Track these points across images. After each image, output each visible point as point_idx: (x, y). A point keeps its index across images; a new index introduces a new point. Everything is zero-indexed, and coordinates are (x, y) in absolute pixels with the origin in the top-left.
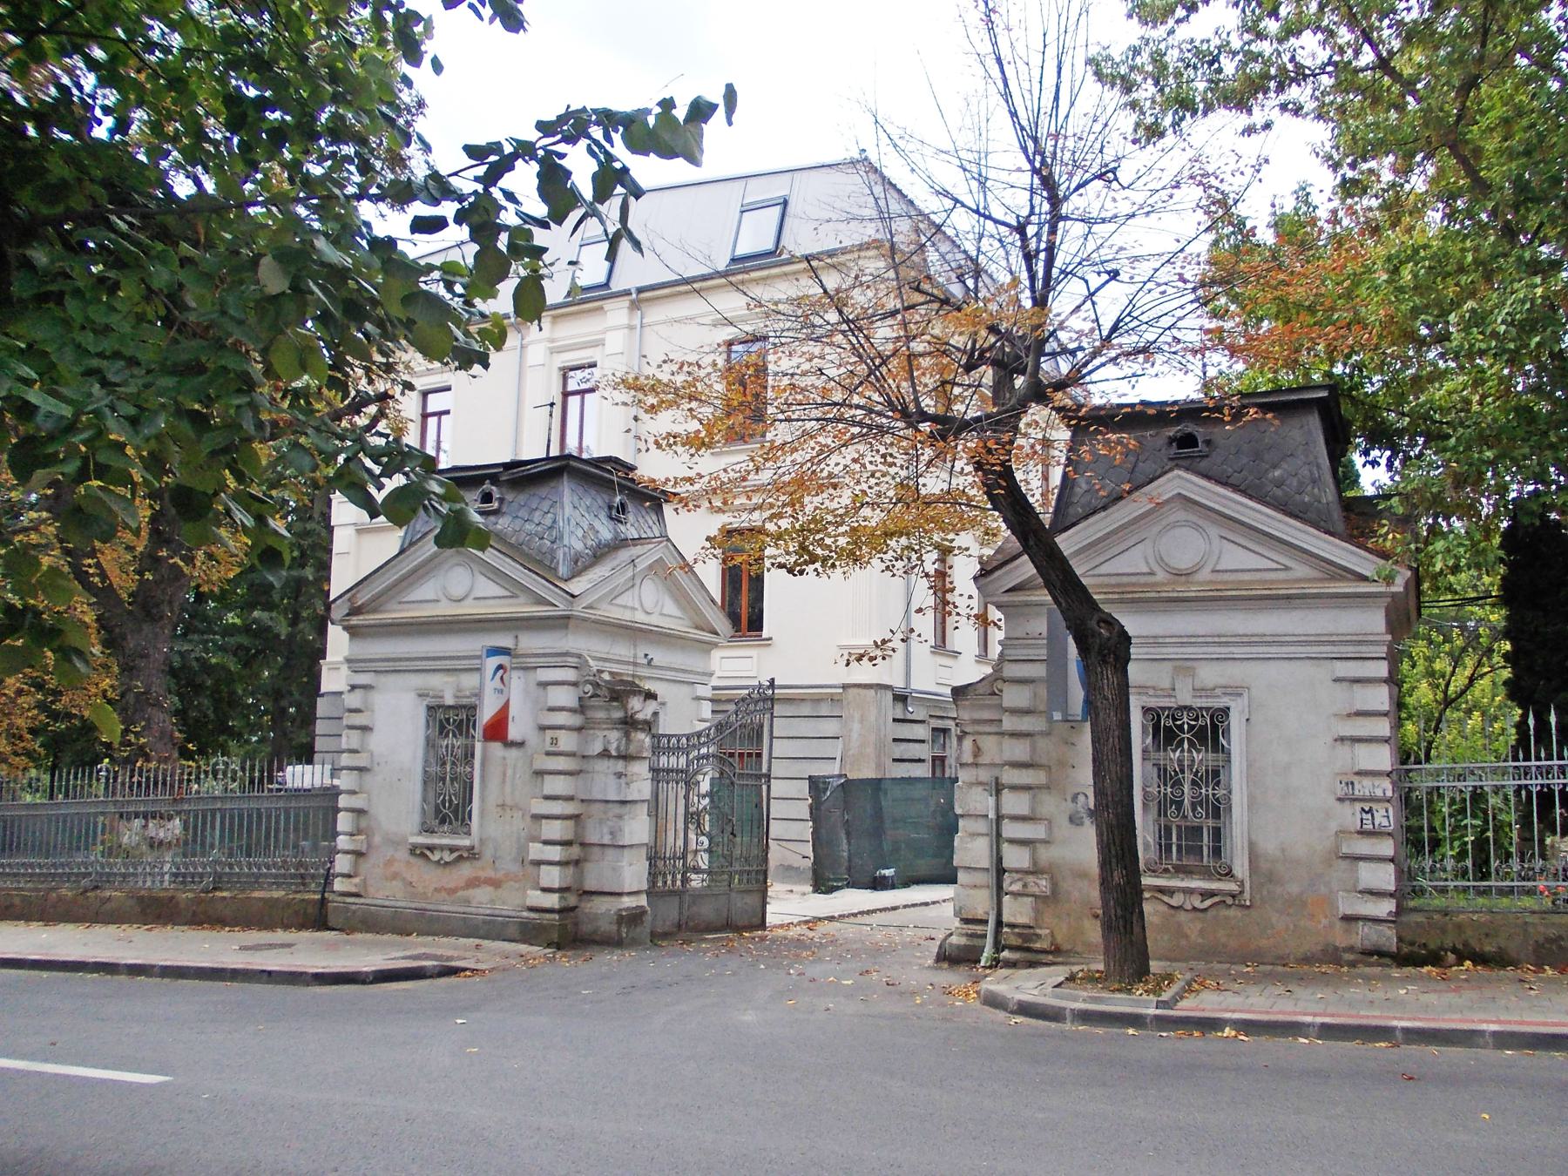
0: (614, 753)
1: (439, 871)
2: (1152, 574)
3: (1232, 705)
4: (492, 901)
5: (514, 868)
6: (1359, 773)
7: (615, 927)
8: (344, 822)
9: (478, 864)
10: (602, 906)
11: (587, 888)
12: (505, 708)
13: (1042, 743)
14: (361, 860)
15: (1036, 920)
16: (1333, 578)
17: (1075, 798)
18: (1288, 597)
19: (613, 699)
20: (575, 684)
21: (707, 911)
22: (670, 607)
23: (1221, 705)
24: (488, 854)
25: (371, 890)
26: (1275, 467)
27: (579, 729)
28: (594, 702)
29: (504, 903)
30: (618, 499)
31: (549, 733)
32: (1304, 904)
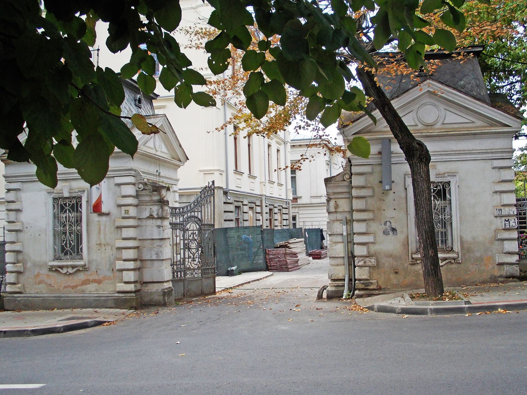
0: (156, 216)
1: (67, 277)
2: (416, 125)
3: (451, 180)
4: (97, 290)
5: (109, 274)
6: (504, 205)
7: (161, 298)
8: (9, 257)
9: (88, 273)
10: (154, 288)
11: (145, 280)
12: (100, 197)
13: (370, 200)
14: (21, 276)
15: (370, 276)
16: (491, 126)
17: (385, 224)
18: (475, 134)
19: (154, 191)
20: (134, 184)
21: (194, 287)
22: (164, 149)
23: (447, 181)
24: (93, 268)
25: (28, 290)
26: (461, 80)
27: (136, 206)
28: (144, 192)
29: (103, 291)
30: (138, 96)
31: (123, 208)
32: (482, 260)
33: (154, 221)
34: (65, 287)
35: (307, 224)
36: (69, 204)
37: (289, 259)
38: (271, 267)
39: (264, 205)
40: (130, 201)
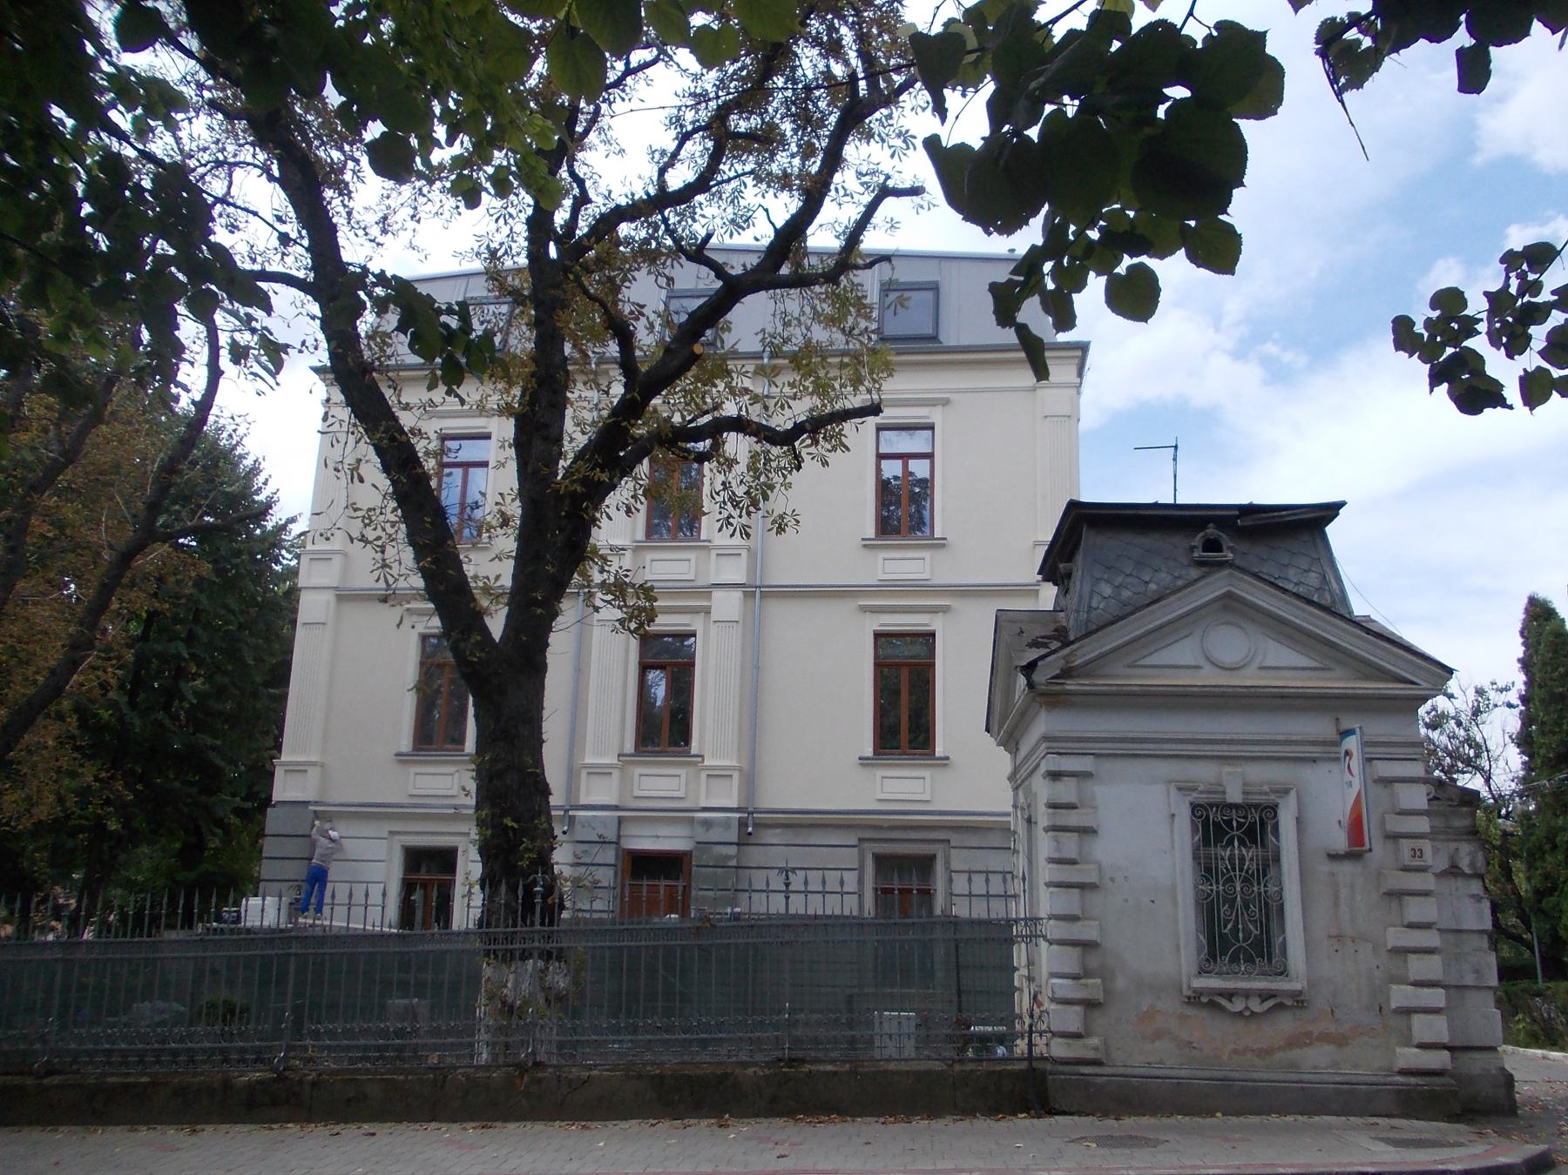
0: (1467, 871)
4: (1335, 1064)
31: (1406, 845)
33: (1460, 882)
34: (1235, 1052)
36: (1240, 825)
40: (1423, 824)
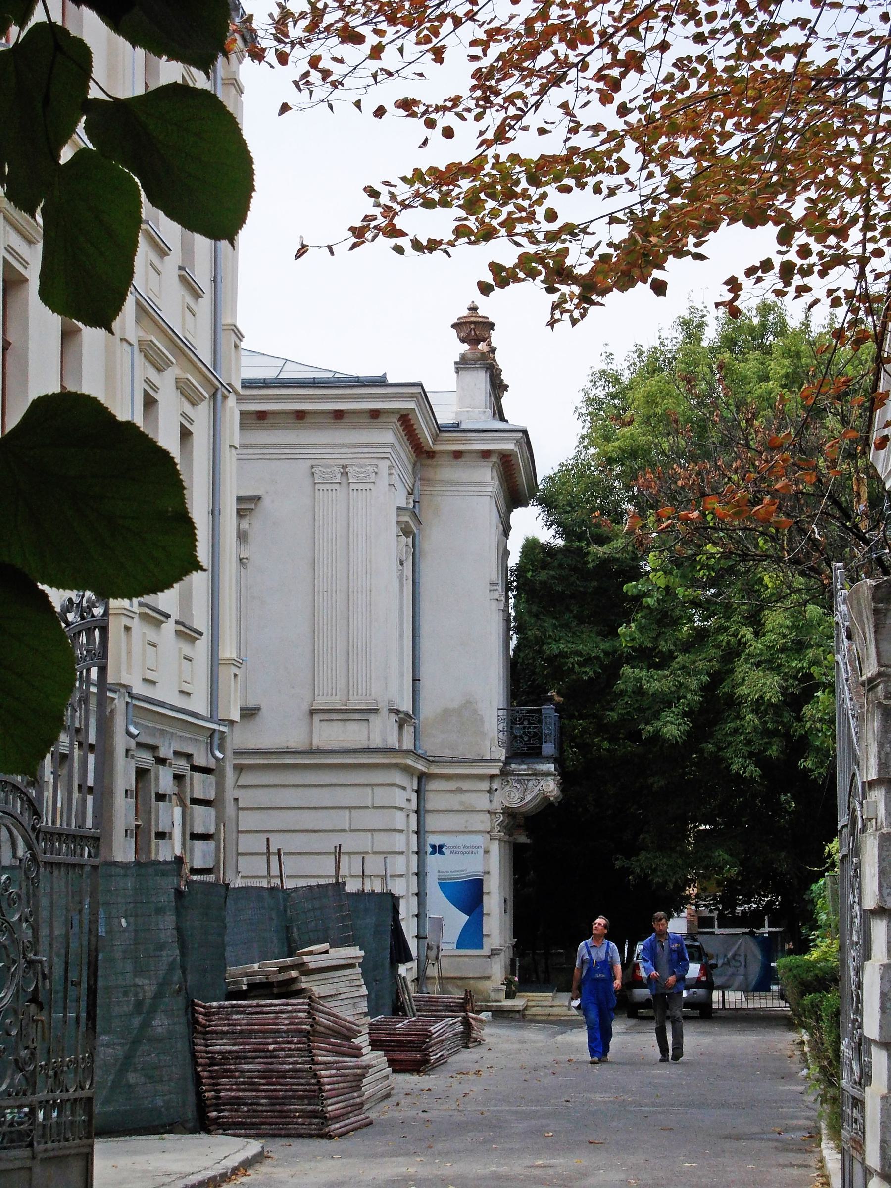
35: (290, 865)
37: (327, 1065)
38: (217, 1108)
39: (121, 742)
